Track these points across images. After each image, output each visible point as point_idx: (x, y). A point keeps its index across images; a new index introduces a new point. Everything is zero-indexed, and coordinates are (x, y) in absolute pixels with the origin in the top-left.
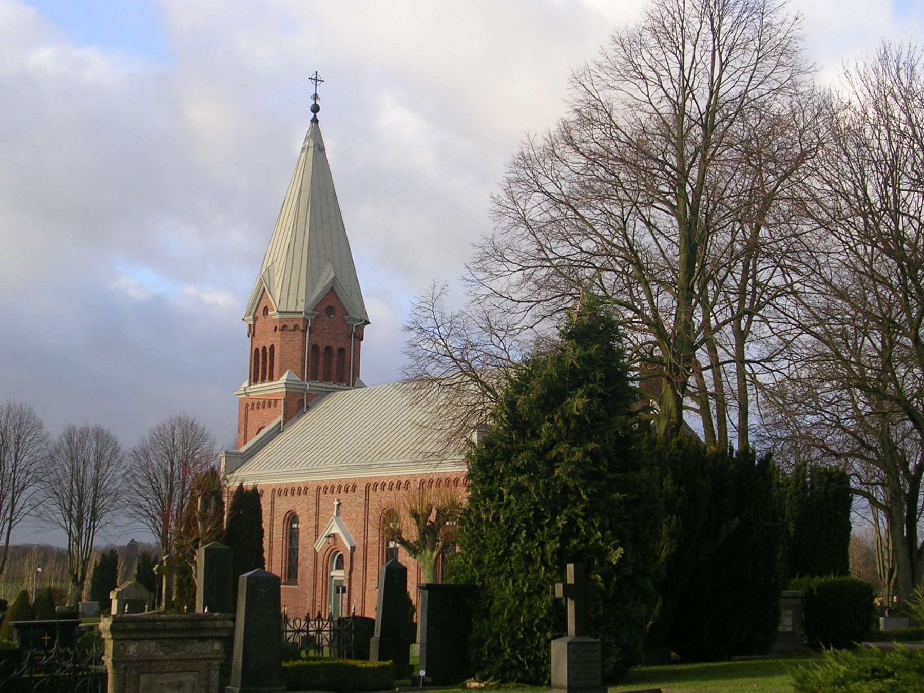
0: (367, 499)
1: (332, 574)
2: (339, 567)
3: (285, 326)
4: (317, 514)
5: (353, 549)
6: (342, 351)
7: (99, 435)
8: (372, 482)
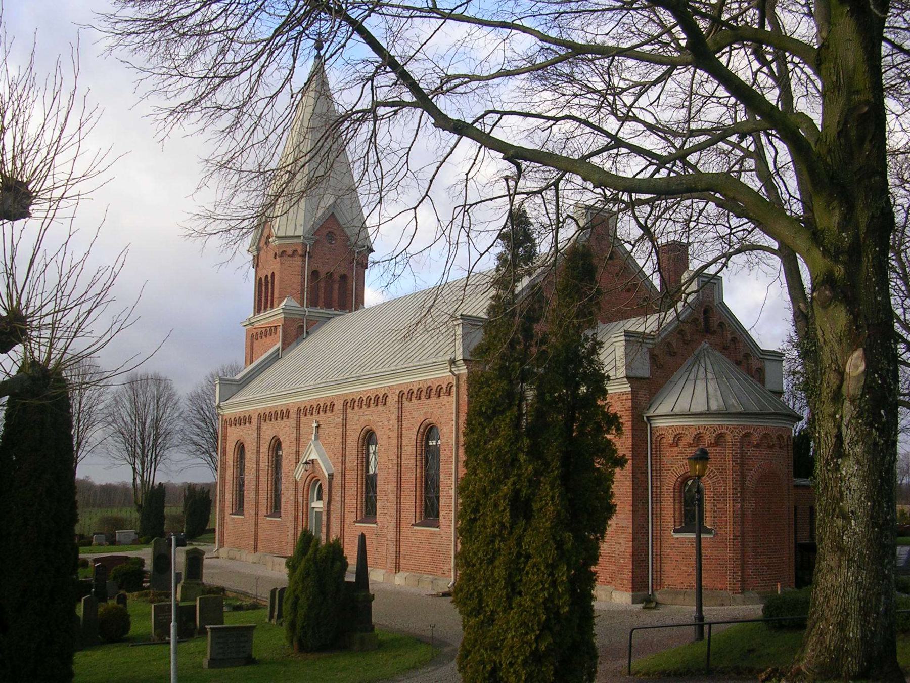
0: (345, 419)
1: (313, 505)
2: (320, 498)
3: (284, 252)
4: (298, 439)
5: (331, 476)
6: (344, 278)
7: (158, 381)
8: (349, 399)
